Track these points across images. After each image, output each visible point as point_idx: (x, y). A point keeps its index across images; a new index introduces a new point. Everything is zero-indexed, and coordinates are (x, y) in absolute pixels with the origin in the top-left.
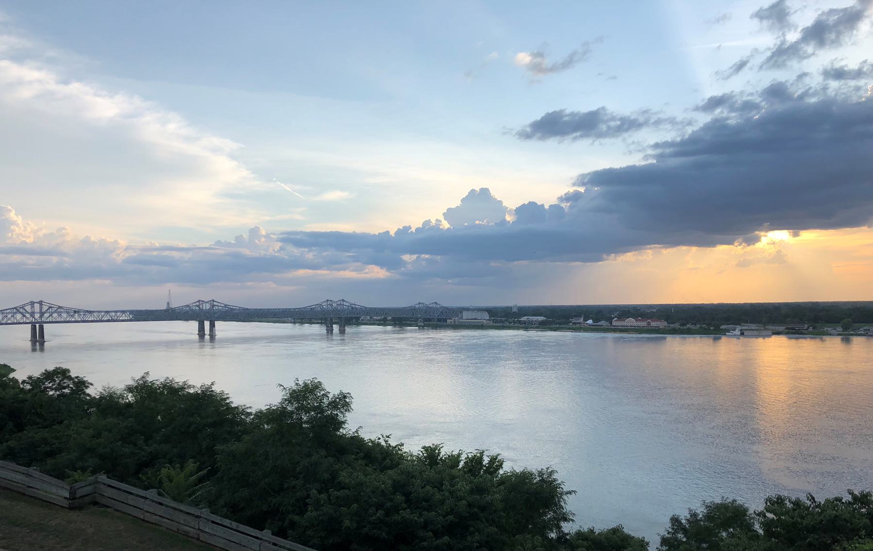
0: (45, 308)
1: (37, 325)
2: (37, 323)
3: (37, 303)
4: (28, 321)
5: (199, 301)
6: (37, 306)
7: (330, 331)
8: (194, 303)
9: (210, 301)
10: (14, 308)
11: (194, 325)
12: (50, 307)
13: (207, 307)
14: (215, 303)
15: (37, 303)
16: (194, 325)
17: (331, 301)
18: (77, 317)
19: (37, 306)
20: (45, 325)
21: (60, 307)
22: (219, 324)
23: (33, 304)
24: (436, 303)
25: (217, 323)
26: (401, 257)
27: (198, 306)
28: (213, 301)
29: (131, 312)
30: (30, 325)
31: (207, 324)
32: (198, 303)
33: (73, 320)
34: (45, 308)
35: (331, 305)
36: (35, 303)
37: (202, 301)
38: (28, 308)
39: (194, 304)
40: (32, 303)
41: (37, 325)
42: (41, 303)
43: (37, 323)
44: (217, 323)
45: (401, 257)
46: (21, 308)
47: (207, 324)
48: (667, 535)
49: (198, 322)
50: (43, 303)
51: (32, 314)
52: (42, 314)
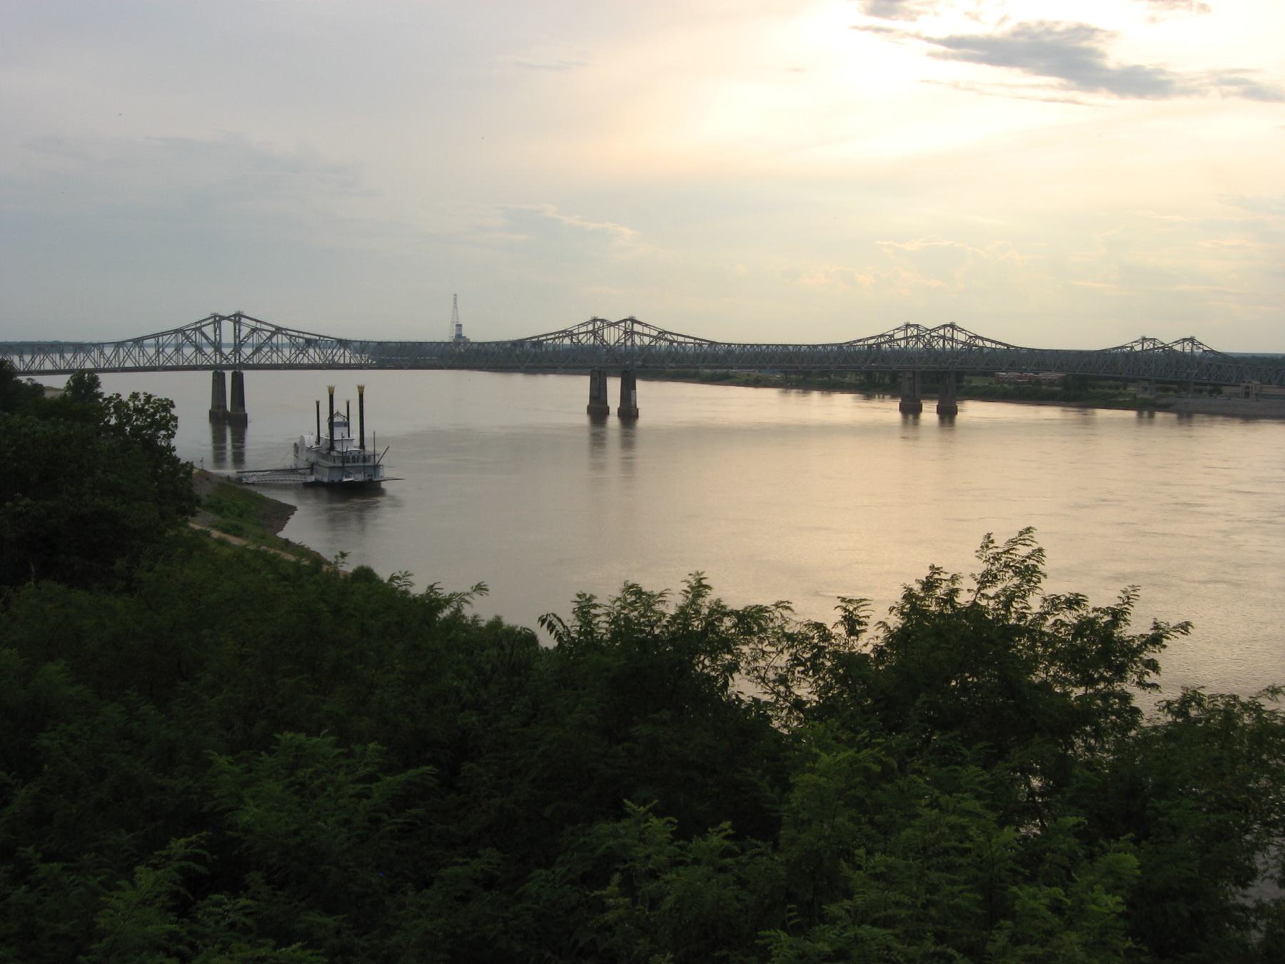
0: (245, 331)
1: (228, 375)
2: (228, 367)
3: (228, 318)
4: (169, 364)
5: (595, 320)
6: (227, 326)
7: (911, 410)
8: (583, 324)
9: (625, 321)
10: (177, 331)
11: (582, 384)
12: (254, 330)
13: (613, 336)
14: (637, 328)
15: (228, 318)
16: (582, 384)
17: (917, 326)
18: (314, 355)
19: (227, 326)
20: (248, 375)
21: (279, 330)
22: (644, 389)
23: (219, 322)
24: (1192, 340)
25: (642, 388)
26: (95, 391)
27: (594, 332)
28: (633, 321)
29: (363, 347)
30: (210, 373)
31: (614, 387)
32: (590, 327)
33: (306, 361)
34: (245, 331)
35: (700, 345)
36: (223, 318)
37: (602, 321)
38: (209, 330)
39: (583, 329)
40: (217, 320)
41: (228, 375)
42: (237, 318)
43: (228, 367)
44: (642, 388)
45: (95, 391)
46: (193, 329)
47: (614, 387)
48: (1163, 718)
49: (620, 379)
50: (243, 320)
51: (217, 347)
52: (238, 347)
